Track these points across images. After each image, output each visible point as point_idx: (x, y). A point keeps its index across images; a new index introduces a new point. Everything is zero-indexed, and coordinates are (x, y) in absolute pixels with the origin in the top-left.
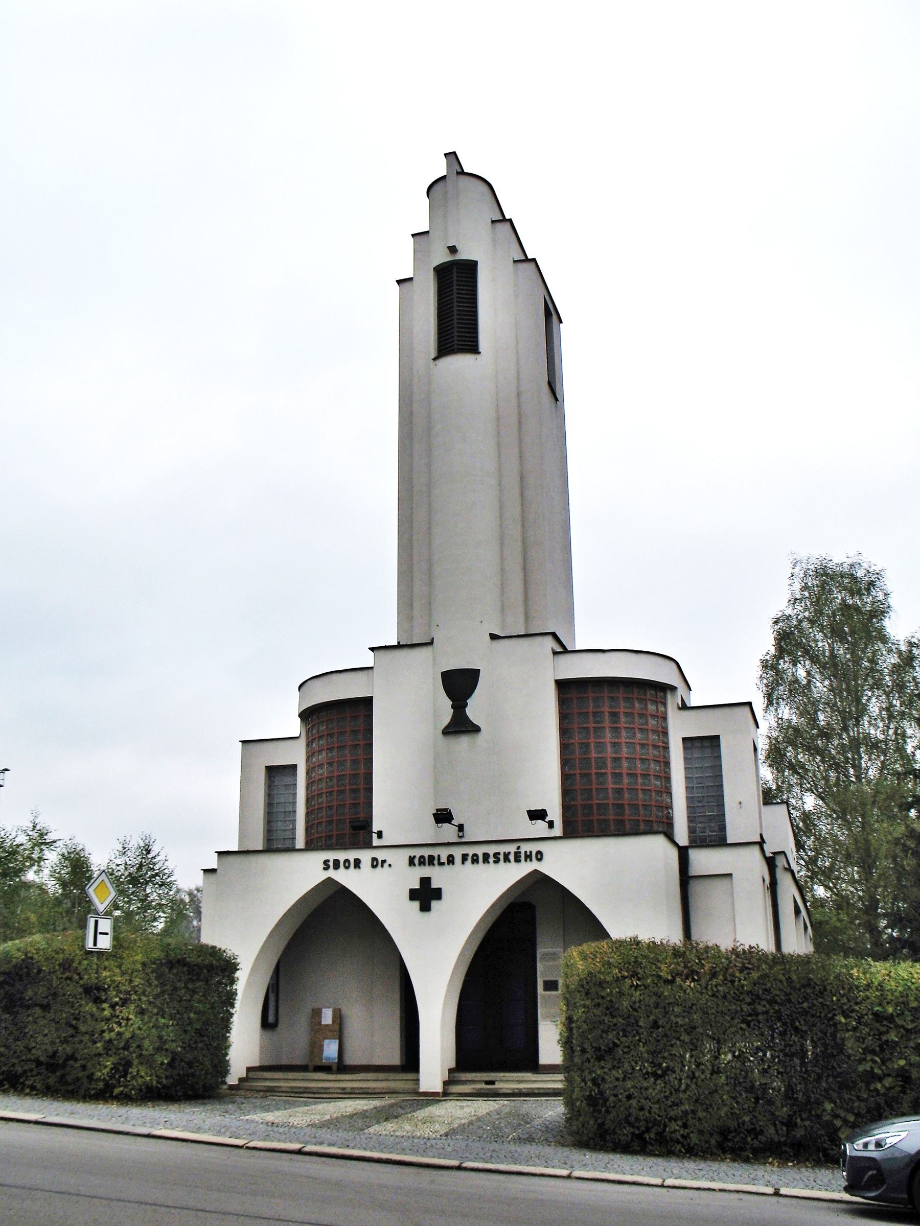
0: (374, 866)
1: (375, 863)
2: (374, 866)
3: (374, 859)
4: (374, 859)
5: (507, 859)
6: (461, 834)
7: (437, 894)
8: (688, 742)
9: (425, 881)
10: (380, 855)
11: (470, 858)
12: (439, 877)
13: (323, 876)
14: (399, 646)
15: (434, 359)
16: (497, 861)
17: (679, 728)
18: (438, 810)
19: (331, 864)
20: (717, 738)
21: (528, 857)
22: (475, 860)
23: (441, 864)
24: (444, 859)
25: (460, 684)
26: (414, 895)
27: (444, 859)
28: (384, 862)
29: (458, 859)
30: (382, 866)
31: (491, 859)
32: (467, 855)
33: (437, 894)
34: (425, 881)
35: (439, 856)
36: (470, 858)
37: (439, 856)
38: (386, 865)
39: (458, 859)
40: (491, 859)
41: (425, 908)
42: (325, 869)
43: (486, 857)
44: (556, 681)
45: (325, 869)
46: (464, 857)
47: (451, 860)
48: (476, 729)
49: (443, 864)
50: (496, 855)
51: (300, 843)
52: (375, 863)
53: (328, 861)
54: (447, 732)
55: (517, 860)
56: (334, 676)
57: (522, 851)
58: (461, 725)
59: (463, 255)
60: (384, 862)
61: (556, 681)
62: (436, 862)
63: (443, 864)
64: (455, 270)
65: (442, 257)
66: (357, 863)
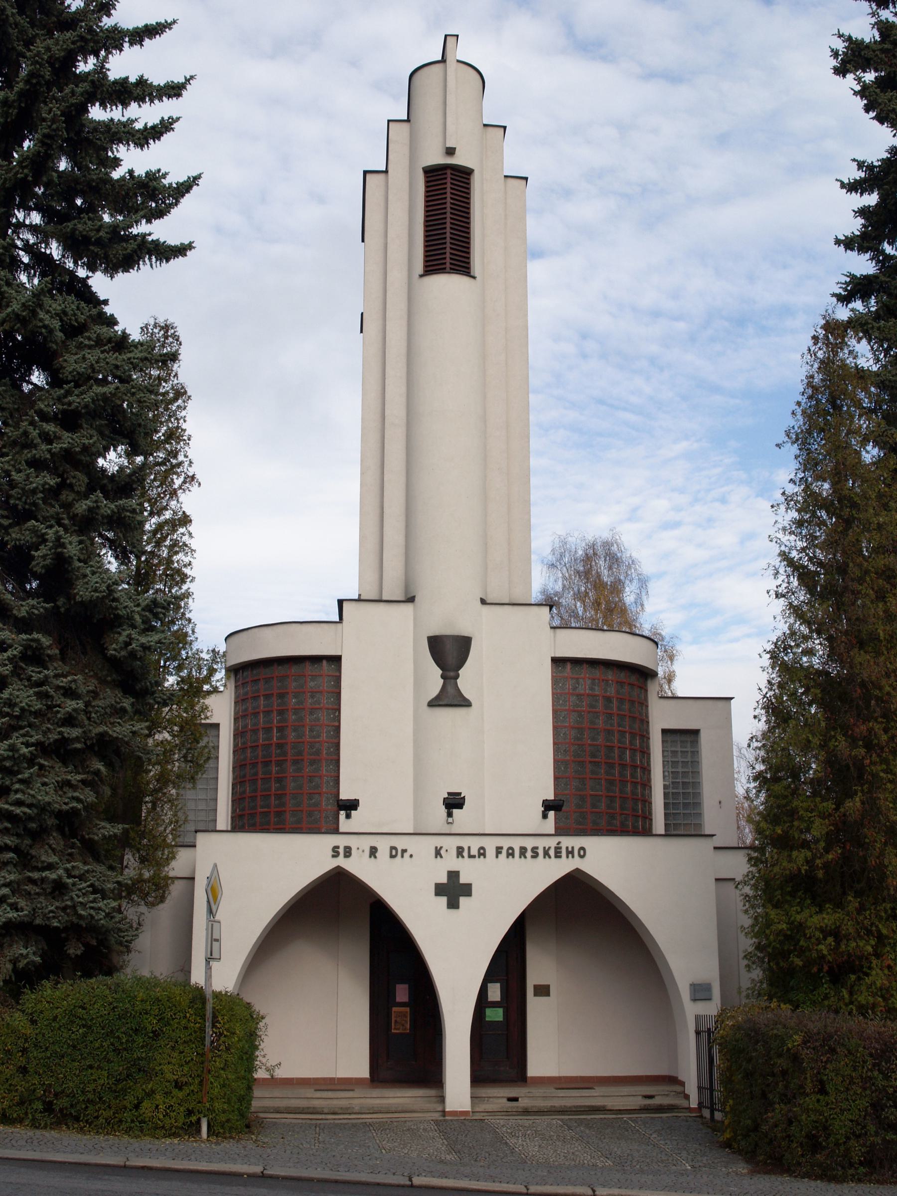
0: (392, 856)
1: (394, 853)
2: (392, 856)
3: (393, 848)
4: (392, 848)
5: (546, 853)
6: (450, 820)
7: (467, 890)
8: (665, 732)
9: (453, 875)
10: (400, 843)
11: (504, 852)
12: (469, 872)
13: (328, 864)
14: (359, 600)
15: (421, 276)
16: (535, 855)
17: (661, 718)
18: (449, 794)
19: (341, 850)
20: (696, 733)
21: (570, 852)
22: (510, 853)
23: (471, 856)
24: (474, 852)
25: (449, 652)
26: (440, 890)
27: (474, 852)
28: (404, 851)
29: (491, 852)
30: (402, 856)
31: (529, 854)
32: (502, 848)
33: (467, 890)
34: (453, 875)
35: (469, 848)
36: (504, 852)
37: (469, 848)
38: (406, 855)
39: (491, 852)
40: (529, 854)
41: (453, 905)
42: (333, 856)
43: (523, 851)
44: (557, 662)
45: (333, 856)
46: (499, 850)
47: (482, 853)
48: (466, 703)
49: (474, 857)
50: (535, 850)
51: (223, 818)
52: (394, 853)
53: (338, 847)
54: (433, 704)
55: (558, 855)
56: (294, 625)
57: (563, 846)
58: (450, 698)
59: (458, 160)
60: (404, 851)
61: (557, 662)
62: (465, 854)
63: (474, 857)
64: (449, 176)
65: (436, 158)
66: (482, 853)
